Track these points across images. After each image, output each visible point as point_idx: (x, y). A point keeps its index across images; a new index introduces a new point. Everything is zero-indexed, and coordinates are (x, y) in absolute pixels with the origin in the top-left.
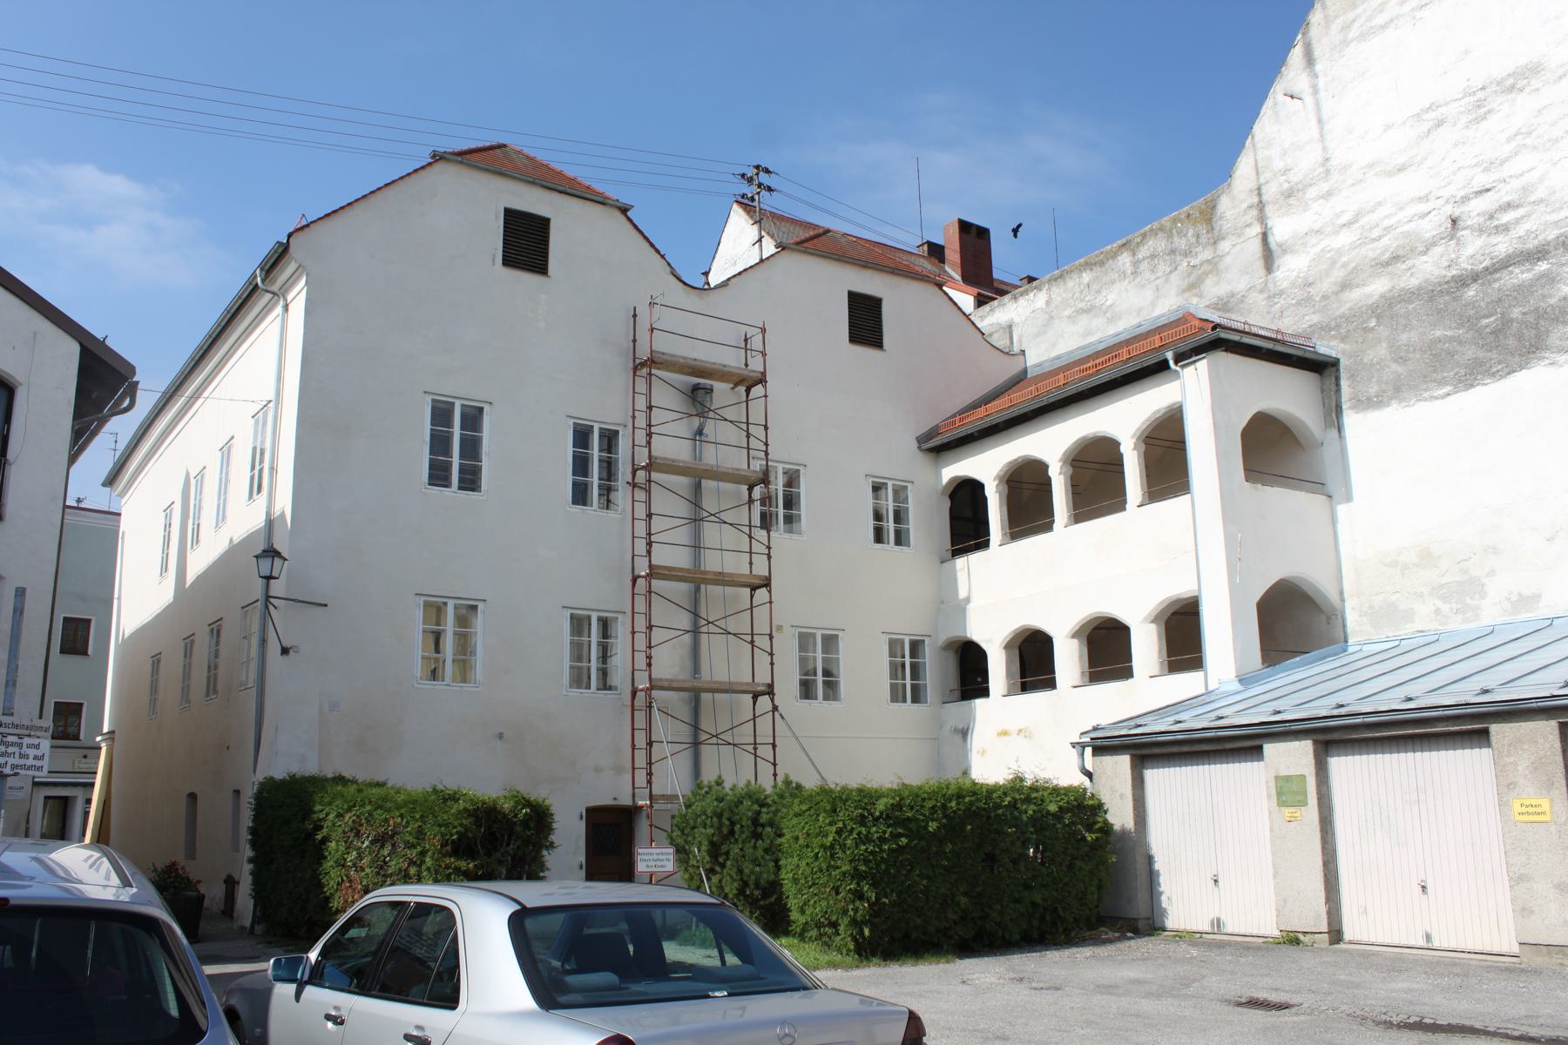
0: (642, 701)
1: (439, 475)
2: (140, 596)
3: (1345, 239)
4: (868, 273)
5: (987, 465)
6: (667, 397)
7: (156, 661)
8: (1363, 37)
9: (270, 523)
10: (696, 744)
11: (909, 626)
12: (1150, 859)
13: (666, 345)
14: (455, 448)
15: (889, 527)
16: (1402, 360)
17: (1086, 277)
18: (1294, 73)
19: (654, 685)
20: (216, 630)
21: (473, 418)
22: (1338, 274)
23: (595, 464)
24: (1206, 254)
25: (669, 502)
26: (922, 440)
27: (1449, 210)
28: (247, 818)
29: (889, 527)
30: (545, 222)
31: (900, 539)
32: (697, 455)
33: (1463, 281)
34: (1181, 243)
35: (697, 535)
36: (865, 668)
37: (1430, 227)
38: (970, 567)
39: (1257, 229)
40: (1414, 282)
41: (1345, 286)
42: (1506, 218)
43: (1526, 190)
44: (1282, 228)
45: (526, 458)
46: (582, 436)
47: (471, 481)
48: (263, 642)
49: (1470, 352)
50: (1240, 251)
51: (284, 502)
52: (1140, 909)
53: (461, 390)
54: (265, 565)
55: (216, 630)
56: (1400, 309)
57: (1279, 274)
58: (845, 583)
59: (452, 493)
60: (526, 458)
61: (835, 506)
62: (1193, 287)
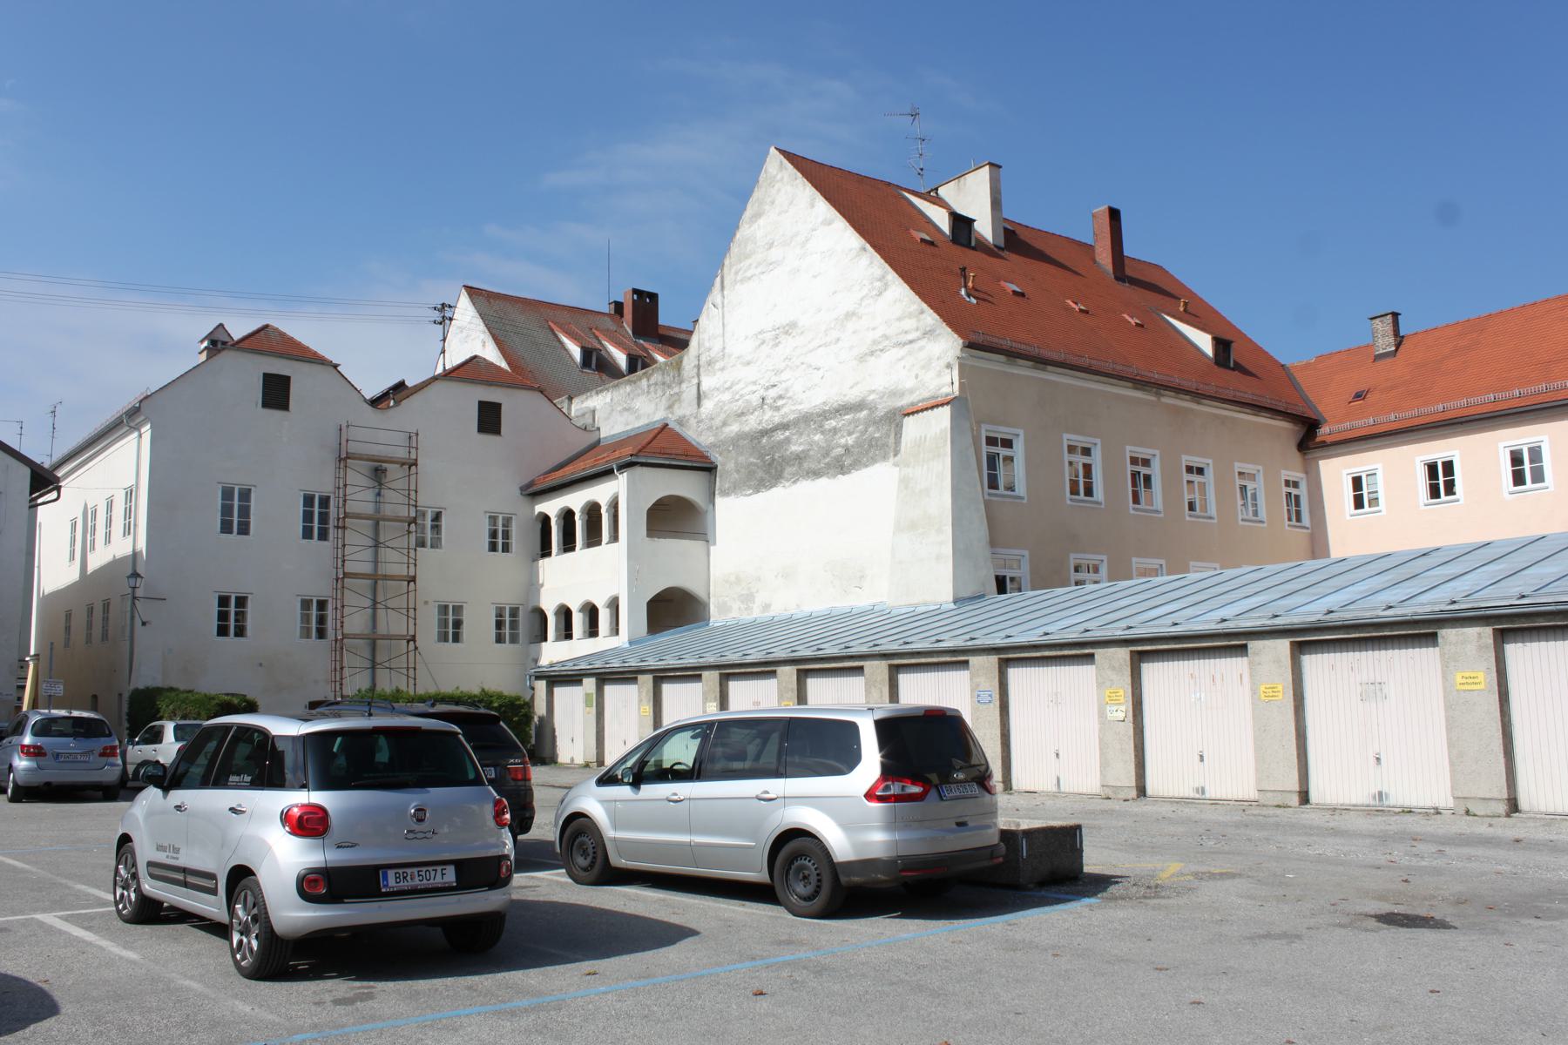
0: (339, 646)
1: (226, 527)
2: (55, 570)
3: (726, 397)
4: (492, 389)
5: (552, 507)
6: (358, 478)
7: (69, 616)
8: (742, 281)
9: (135, 555)
10: (373, 668)
11: (508, 599)
12: (554, 730)
13: (353, 448)
14: (236, 514)
15: (498, 541)
16: (738, 471)
17: (628, 388)
18: (715, 295)
19: (344, 636)
20: (106, 606)
21: (245, 495)
22: (723, 416)
23: (319, 517)
24: (676, 390)
25: (357, 538)
26: (522, 489)
27: (762, 392)
28: (125, 708)
29: (498, 541)
30: (288, 379)
31: (506, 548)
32: (378, 510)
33: (765, 433)
34: (668, 379)
35: (376, 554)
36: (480, 624)
37: (755, 400)
38: (544, 563)
39: (695, 381)
40: (747, 429)
41: (725, 424)
42: (780, 403)
43: (787, 390)
44: (707, 383)
45: (276, 513)
46: (308, 500)
47: (244, 529)
48: (133, 618)
49: (760, 474)
50: (689, 391)
51: (142, 545)
52: (547, 753)
53: (238, 480)
54: (132, 581)
55: (106, 606)
56: (741, 443)
57: (702, 409)
58: (464, 573)
59: (234, 537)
60: (276, 513)
61: (465, 530)
62: (670, 407)
